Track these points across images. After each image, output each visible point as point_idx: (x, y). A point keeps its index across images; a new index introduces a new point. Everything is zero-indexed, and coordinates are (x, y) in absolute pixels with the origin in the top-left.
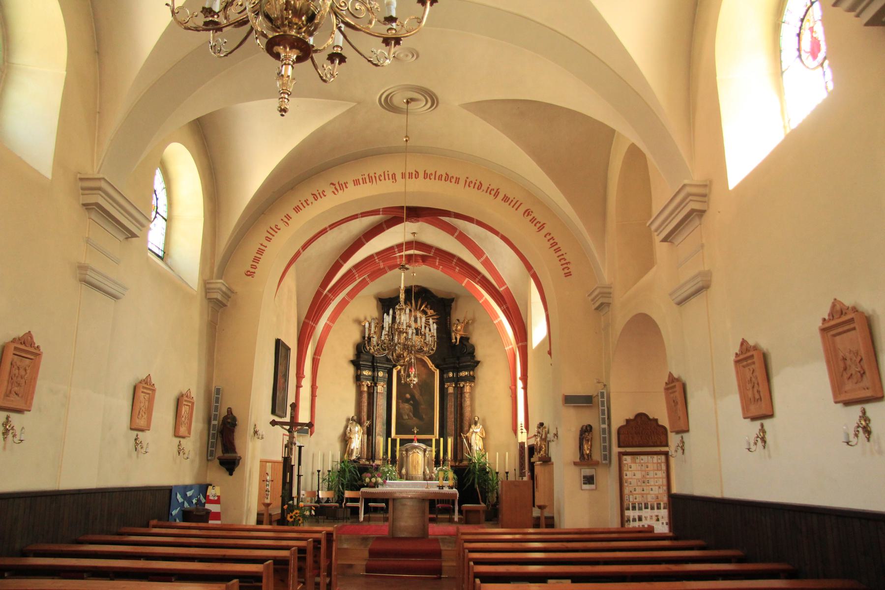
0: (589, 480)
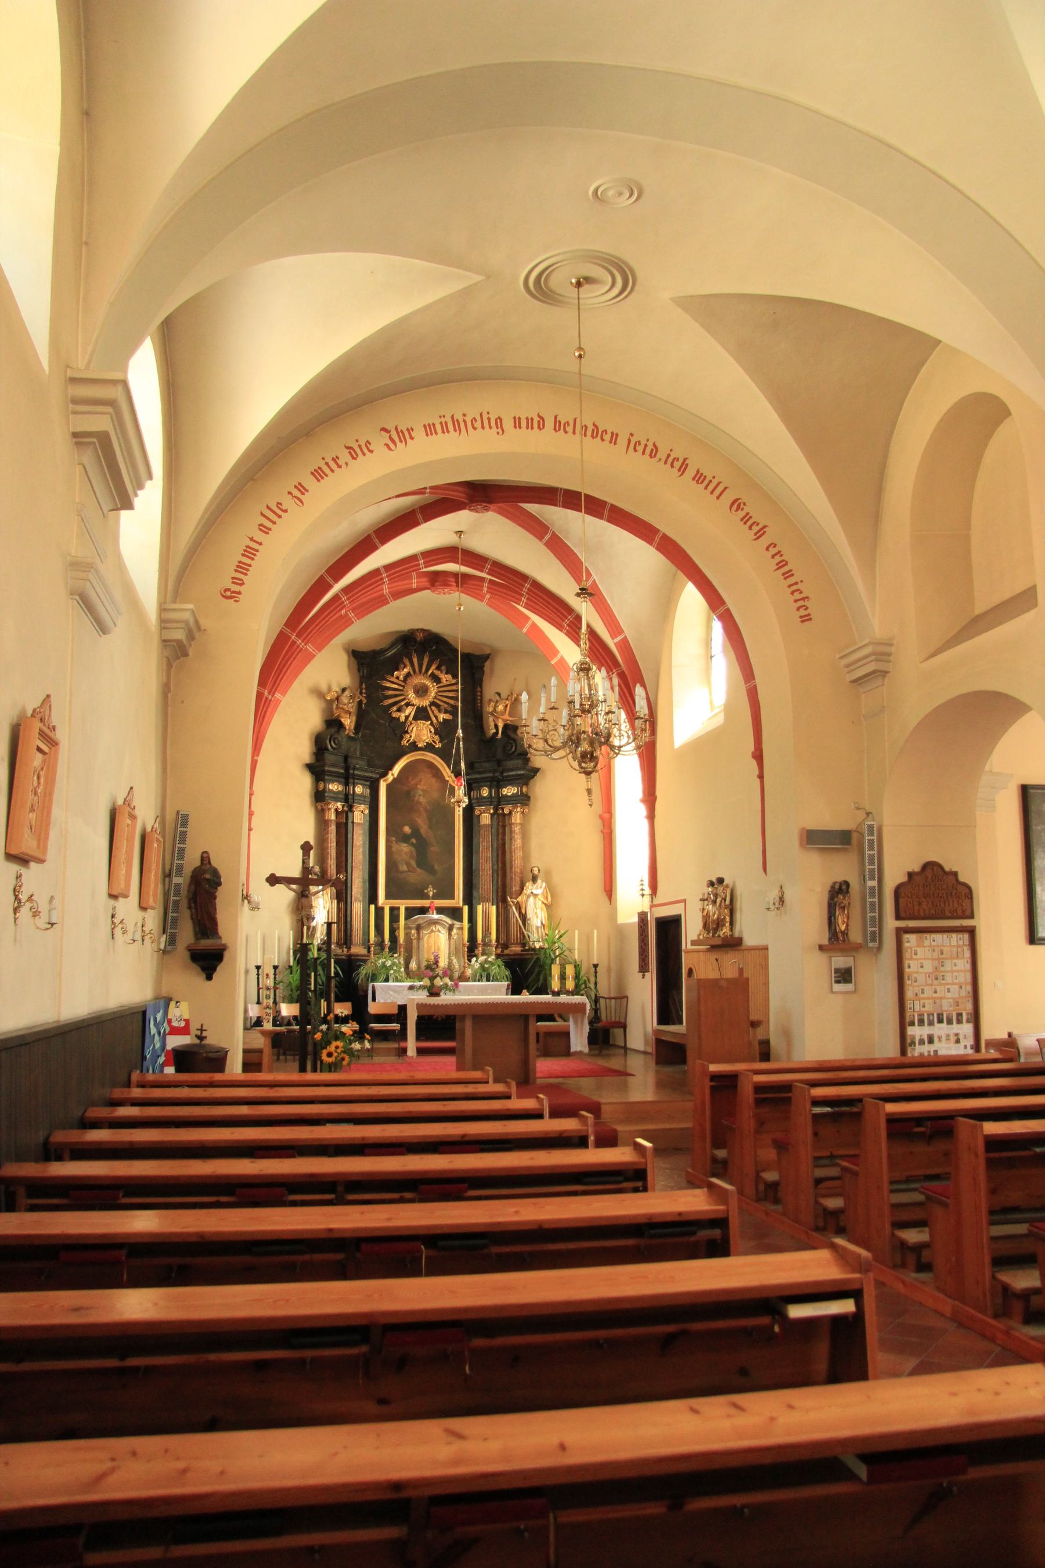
0: (844, 976)
